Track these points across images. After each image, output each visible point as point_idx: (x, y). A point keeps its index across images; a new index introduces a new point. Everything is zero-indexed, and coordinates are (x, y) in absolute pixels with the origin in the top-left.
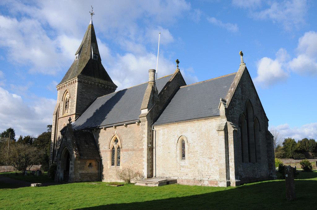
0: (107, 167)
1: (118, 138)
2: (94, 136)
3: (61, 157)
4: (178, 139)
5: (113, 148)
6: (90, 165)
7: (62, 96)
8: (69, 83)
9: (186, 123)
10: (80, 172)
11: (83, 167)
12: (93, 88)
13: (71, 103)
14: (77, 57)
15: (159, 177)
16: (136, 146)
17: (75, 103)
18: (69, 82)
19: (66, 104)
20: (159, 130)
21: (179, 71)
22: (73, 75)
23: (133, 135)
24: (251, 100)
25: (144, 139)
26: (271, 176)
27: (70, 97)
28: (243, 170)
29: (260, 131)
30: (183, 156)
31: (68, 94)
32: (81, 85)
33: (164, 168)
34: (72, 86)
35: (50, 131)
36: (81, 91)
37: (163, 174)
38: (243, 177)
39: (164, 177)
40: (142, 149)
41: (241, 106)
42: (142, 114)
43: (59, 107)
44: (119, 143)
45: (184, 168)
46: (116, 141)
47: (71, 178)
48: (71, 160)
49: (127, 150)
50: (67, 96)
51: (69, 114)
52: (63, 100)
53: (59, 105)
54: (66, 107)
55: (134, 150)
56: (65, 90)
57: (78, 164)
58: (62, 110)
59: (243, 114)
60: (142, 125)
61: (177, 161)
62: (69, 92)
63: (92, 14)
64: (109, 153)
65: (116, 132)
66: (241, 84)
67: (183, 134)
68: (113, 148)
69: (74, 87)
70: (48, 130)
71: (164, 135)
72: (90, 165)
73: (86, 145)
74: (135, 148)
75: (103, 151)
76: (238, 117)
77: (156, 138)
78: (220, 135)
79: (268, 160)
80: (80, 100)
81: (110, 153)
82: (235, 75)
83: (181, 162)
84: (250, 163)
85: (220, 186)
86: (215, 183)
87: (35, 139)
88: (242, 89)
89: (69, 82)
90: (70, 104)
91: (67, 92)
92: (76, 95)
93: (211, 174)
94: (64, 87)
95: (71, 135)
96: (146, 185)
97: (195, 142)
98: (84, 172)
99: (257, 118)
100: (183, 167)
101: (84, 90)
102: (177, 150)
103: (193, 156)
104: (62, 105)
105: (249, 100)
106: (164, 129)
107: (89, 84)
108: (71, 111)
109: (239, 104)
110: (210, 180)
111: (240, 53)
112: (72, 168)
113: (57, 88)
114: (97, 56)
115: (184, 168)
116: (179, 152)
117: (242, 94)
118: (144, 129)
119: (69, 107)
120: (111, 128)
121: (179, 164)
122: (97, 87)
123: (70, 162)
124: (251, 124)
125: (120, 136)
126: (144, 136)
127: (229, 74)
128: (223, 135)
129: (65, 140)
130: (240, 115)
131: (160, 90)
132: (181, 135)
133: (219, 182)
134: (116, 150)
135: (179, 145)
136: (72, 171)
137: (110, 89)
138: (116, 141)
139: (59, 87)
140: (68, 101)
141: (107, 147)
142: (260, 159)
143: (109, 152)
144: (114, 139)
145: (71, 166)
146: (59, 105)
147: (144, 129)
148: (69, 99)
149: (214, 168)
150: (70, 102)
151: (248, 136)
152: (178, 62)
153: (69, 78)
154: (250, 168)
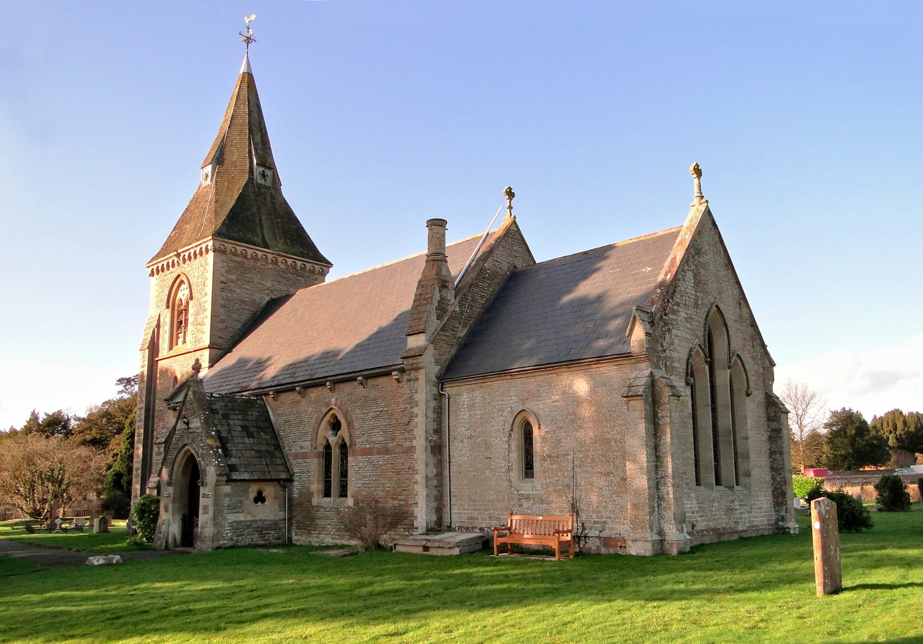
1: (343, 421)
2: (271, 413)
3: (174, 477)
4: (511, 420)
5: (328, 447)
6: (260, 498)
7: (167, 292)
8: (187, 254)
9: (535, 374)
10: (232, 518)
11: (241, 502)
12: (260, 268)
13: (197, 314)
14: (207, 176)
15: (460, 528)
16: (393, 439)
17: (208, 313)
19: (178, 317)
20: (459, 394)
21: (514, 222)
22: (197, 229)
23: (385, 409)
24: (722, 307)
25: (416, 420)
26: (781, 523)
27: (191, 298)
28: (700, 508)
29: (748, 395)
30: (528, 469)
31: (183, 286)
32: (223, 261)
33: (474, 501)
34: (196, 263)
35: (777, 508)
36: (224, 279)
37: (471, 518)
38: (700, 526)
39: (474, 528)
40: (412, 449)
41: (691, 325)
42: (410, 350)
44: (344, 431)
45: (532, 502)
46: (336, 426)
47: (205, 537)
48: (202, 485)
49: (367, 452)
51: (189, 346)
52: (171, 304)
53: (159, 321)
54: (179, 327)
55: (387, 451)
56: (175, 275)
57: (226, 495)
59: (699, 349)
60: (409, 380)
61: (510, 481)
62: (185, 280)
63: (248, 40)
64: (316, 460)
65: (333, 400)
66: (694, 262)
67: (527, 406)
68: (328, 447)
69: (202, 269)
70: (121, 392)
71: (472, 407)
72: (260, 498)
73: (247, 440)
75: (297, 456)
76: (686, 357)
77: (451, 416)
78: (630, 410)
79: (773, 478)
80: (223, 306)
81: (319, 463)
82: (675, 235)
83: (521, 485)
84: (719, 488)
85: (634, 554)
86: (619, 544)
87: (79, 419)
88: (696, 276)
90: (191, 319)
91: (182, 282)
92: (209, 289)
93: (608, 517)
94: (171, 268)
95: (200, 413)
97: (561, 428)
98: (241, 517)
99: (741, 360)
100: (528, 498)
101: (234, 277)
102: (509, 452)
103: (555, 466)
104: (168, 320)
105: (717, 306)
106: (473, 390)
107: (249, 257)
108: (197, 341)
109: (688, 319)
110: (604, 534)
111: (692, 168)
112: (206, 508)
113: (150, 270)
114: (268, 172)
115: (532, 502)
116: (516, 457)
117: (696, 291)
118: (416, 392)
119: (190, 328)
121: (518, 491)
122: (271, 266)
123: (201, 488)
124: (723, 376)
125: (347, 411)
126: (416, 410)
127: (660, 230)
128: (641, 411)
129: (185, 426)
130: (691, 350)
131: (457, 267)
132: (521, 408)
133: (629, 543)
134: (336, 452)
135: (517, 437)
137: (312, 272)
139: (155, 267)
140: (186, 310)
141: (308, 443)
142: (748, 474)
143: (315, 457)
144: (329, 421)
145: (203, 502)
146: (159, 321)
147: (416, 392)
148: (188, 303)
149: (615, 501)
150: (191, 311)
151: (714, 410)
152: (510, 194)
153: (184, 241)
154: (718, 502)
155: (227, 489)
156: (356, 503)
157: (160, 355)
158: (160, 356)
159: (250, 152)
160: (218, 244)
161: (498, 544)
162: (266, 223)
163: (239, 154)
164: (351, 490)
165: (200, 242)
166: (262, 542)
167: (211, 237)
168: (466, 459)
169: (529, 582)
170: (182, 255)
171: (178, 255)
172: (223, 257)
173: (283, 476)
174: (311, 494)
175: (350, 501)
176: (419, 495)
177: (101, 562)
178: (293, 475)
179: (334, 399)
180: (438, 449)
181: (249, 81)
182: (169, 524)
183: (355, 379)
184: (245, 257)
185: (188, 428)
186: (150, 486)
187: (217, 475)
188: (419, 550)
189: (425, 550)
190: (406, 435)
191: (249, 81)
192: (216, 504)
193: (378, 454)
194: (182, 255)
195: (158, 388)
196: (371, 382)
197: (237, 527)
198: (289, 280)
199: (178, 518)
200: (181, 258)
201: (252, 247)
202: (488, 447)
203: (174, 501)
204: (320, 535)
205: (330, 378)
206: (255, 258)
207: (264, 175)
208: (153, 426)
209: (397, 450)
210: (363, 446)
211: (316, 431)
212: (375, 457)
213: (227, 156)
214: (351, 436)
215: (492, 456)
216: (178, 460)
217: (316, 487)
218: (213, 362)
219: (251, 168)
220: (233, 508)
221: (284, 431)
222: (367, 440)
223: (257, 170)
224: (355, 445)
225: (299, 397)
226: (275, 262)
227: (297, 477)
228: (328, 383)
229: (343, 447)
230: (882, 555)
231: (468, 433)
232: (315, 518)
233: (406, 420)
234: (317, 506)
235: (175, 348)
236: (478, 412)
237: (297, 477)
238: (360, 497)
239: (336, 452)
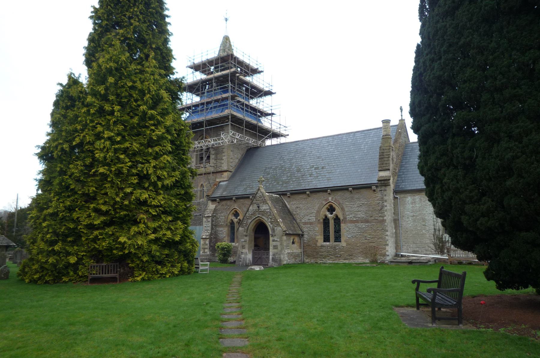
33: (416, 244)
55: (367, 221)
134: (332, 223)
161: (91, 278)
168: (411, 225)
169: (211, 288)
178: (304, 232)
180: (396, 221)
183: (232, 199)
202: (424, 220)
210: (352, 219)
215: (426, 224)
222: (354, 217)
229: (337, 220)
231: (412, 214)
233: (379, 208)
236: (418, 205)
237: (306, 233)
239: (332, 223)
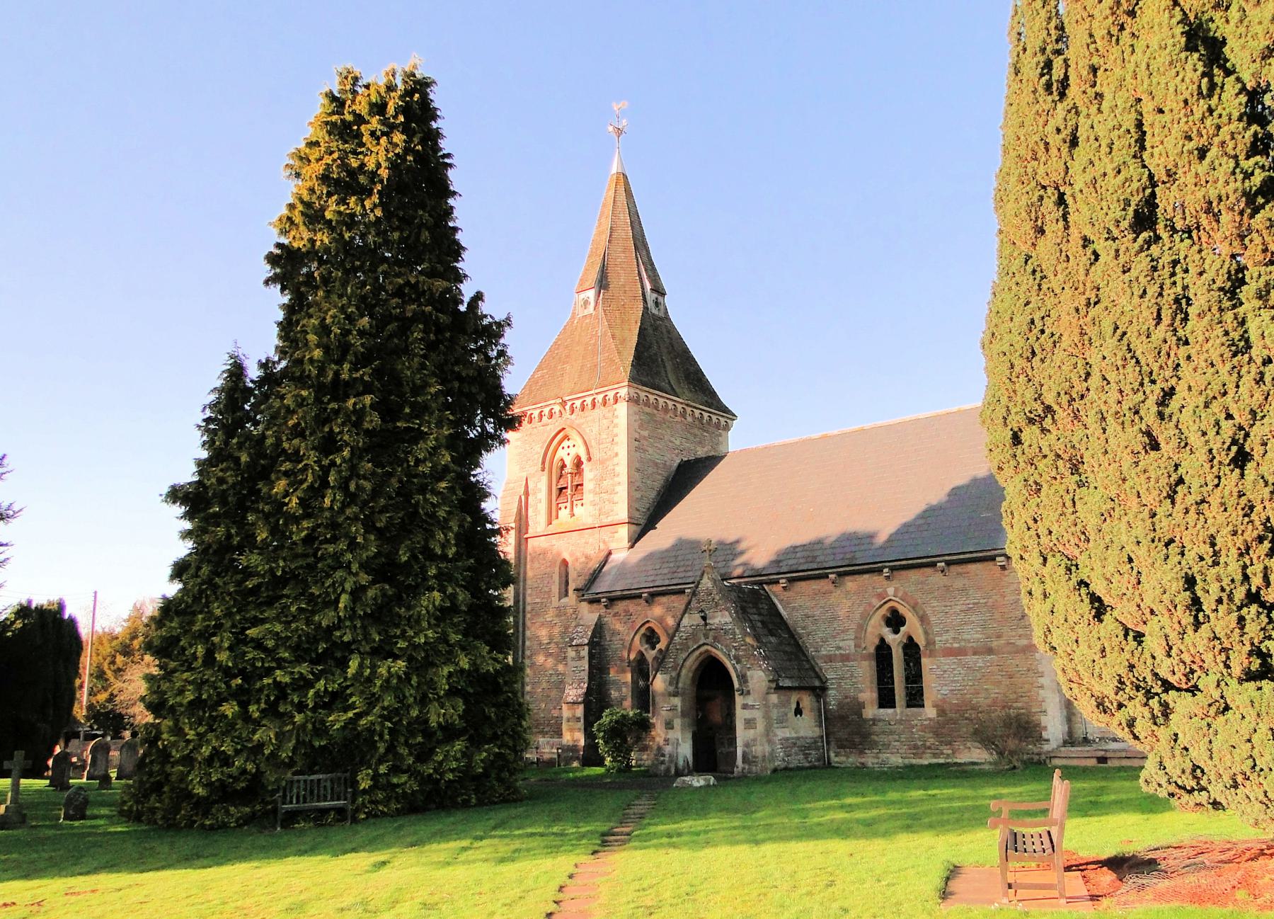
0: (361, 666)
2: (780, 607)
18: (578, 398)
30: (96, 593)
43: (527, 494)
50: (566, 454)
55: (990, 651)
58: (543, 507)
74: (995, 644)
75: (830, 659)
80: (638, 470)
89: (578, 398)
91: (566, 437)
94: (545, 419)
96: (1099, 762)
120: (866, 576)
122: (678, 419)
136: (752, 731)
138: (895, 621)
141: (852, 643)
155: (774, 698)
156: (942, 712)
157: (530, 531)
158: (531, 532)
159: (639, 274)
160: (632, 391)
162: (669, 366)
163: (625, 273)
164: (930, 696)
165: (606, 388)
166: (807, 765)
167: (626, 383)
170: (569, 404)
171: (564, 403)
172: (636, 408)
173: (817, 683)
174: (861, 706)
175: (930, 712)
176: (1047, 700)
177: (702, 783)
179: (894, 590)
181: (624, 180)
182: (678, 744)
184: (656, 408)
185: (706, 624)
186: (569, 699)
187: (770, 681)
188: (1093, 762)
189: (1099, 762)
190: (1021, 631)
191: (624, 180)
192: (767, 716)
193: (975, 654)
194: (569, 404)
195: (530, 574)
196: (954, 569)
197: (789, 744)
198: (695, 436)
199: (689, 736)
200: (568, 407)
201: (664, 395)
203: (684, 715)
204: (880, 755)
205: (887, 564)
206: (666, 409)
207: (657, 304)
208: (524, 624)
209: (1009, 648)
211: (861, 628)
212: (970, 659)
213: (612, 278)
214: (926, 633)
216: (688, 663)
217: (868, 695)
218: (635, 540)
219: (644, 295)
220: (782, 721)
221: (803, 628)
223: (651, 297)
224: (934, 643)
225: (831, 587)
226: (684, 415)
227: (832, 684)
228: (886, 570)
229: (911, 649)
230: (459, 839)
232: (870, 734)
234: (874, 720)
235: (555, 522)
238: (947, 707)
